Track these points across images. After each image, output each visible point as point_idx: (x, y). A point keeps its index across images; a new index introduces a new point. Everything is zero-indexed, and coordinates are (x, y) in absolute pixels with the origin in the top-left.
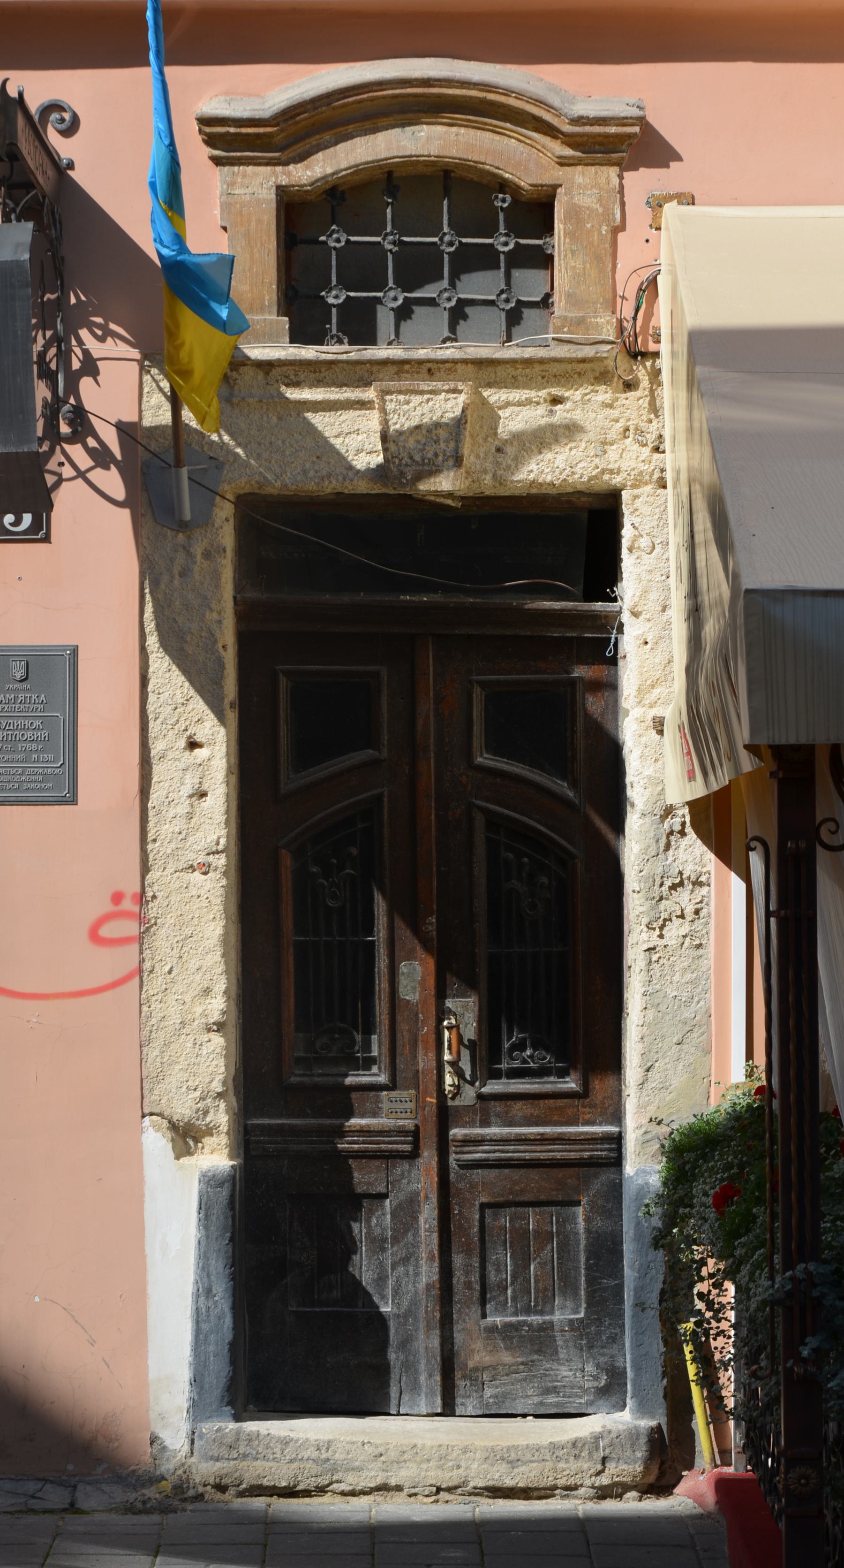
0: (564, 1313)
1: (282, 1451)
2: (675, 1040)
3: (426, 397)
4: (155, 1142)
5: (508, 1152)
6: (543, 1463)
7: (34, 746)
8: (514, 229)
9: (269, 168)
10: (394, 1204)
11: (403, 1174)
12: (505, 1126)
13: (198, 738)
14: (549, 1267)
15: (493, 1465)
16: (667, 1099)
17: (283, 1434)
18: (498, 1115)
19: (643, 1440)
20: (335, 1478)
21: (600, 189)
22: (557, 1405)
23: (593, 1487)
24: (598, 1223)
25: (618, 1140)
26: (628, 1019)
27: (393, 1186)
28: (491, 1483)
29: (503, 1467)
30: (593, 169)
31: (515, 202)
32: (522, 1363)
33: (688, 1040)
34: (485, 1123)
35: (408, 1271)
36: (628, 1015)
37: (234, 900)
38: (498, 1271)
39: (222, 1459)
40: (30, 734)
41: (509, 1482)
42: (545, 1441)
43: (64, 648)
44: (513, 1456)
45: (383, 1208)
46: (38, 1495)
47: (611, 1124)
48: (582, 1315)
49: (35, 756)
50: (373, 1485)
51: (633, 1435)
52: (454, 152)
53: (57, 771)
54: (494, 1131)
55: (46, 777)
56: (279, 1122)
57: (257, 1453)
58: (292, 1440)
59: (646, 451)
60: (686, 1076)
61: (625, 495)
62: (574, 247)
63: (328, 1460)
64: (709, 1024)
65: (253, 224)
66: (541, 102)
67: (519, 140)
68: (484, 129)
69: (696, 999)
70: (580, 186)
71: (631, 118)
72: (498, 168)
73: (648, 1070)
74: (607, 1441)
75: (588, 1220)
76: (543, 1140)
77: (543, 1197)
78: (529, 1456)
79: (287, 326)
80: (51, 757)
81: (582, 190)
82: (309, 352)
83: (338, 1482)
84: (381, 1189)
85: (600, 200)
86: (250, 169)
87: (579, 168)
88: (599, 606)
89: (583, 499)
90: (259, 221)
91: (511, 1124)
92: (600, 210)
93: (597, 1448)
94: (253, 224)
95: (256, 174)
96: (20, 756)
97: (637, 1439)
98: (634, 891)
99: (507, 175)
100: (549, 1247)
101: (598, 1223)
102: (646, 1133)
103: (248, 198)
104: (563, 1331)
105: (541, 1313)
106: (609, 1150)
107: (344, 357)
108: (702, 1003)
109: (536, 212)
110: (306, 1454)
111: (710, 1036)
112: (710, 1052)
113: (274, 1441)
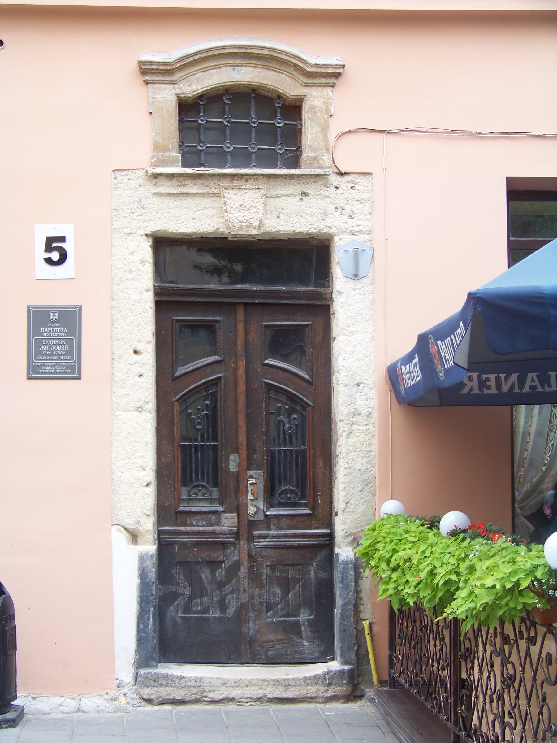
0: (304, 617)
1: (179, 682)
2: (359, 489)
3: (245, 191)
4: (119, 538)
5: (279, 541)
6: (300, 687)
7: (61, 353)
8: (284, 117)
9: (171, 86)
10: (227, 566)
11: (231, 552)
12: (277, 530)
13: (138, 349)
14: (298, 595)
15: (277, 688)
16: (356, 517)
17: (179, 674)
18: (274, 525)
19: (346, 675)
20: (203, 695)
21: (324, 98)
22: (301, 658)
23: (323, 697)
24: (321, 574)
25: (331, 537)
26: (336, 481)
27: (227, 558)
28: (276, 696)
29: (282, 688)
30: (320, 89)
31: (283, 105)
32: (286, 639)
33: (365, 490)
34: (269, 528)
35: (233, 597)
36: (336, 478)
37: (175, 236)
38: (274, 596)
39: (151, 686)
40: (59, 347)
41: (284, 696)
42: (301, 676)
43: (76, 307)
44: (286, 683)
45: (221, 568)
46: (62, 704)
47: (325, 528)
48: (313, 617)
49: (62, 357)
50: (221, 698)
51: (341, 673)
52: (257, 80)
53: (72, 364)
54: (272, 532)
55: (67, 367)
56: (174, 528)
57: (167, 683)
58: (183, 677)
59: (345, 218)
60: (364, 506)
61: (336, 238)
62: (312, 124)
63: (200, 686)
64: (375, 482)
65: (164, 111)
66: (298, 57)
67: (286, 75)
68: (270, 70)
69: (369, 470)
70: (314, 97)
71: (339, 65)
72: (277, 88)
73: (346, 503)
74: (330, 675)
75: (315, 573)
76: (295, 536)
77: (295, 562)
78: (293, 683)
79: (180, 159)
80: (70, 358)
81: (315, 99)
82: (190, 171)
83: (204, 697)
84: (221, 559)
85: (324, 103)
86: (163, 86)
87: (315, 88)
88: (321, 290)
89: (315, 241)
90: (167, 110)
91: (281, 529)
92: (324, 108)
93: (326, 679)
94: (164, 111)
95: (166, 89)
96: (56, 357)
97: (344, 674)
98: (340, 421)
99: (281, 91)
100: (298, 585)
101: (321, 574)
102: (346, 532)
103: (161, 99)
104: (304, 624)
105: (295, 616)
106: (326, 541)
107: (207, 172)
108: (372, 472)
109: (293, 109)
110: (189, 684)
111: (375, 487)
112: (375, 495)
113: (175, 677)
